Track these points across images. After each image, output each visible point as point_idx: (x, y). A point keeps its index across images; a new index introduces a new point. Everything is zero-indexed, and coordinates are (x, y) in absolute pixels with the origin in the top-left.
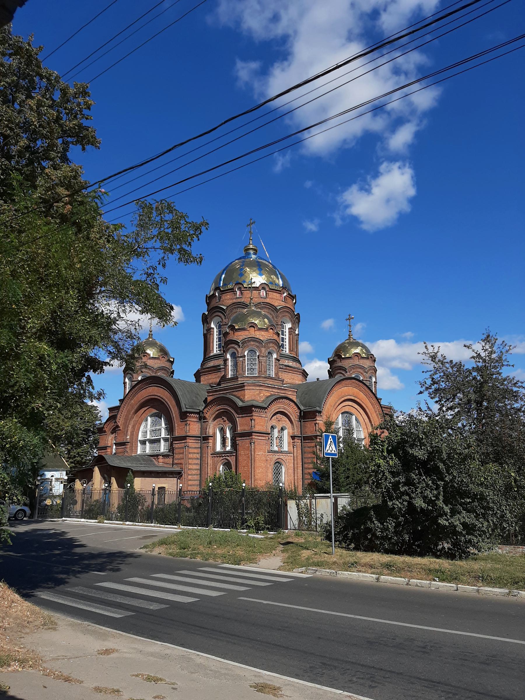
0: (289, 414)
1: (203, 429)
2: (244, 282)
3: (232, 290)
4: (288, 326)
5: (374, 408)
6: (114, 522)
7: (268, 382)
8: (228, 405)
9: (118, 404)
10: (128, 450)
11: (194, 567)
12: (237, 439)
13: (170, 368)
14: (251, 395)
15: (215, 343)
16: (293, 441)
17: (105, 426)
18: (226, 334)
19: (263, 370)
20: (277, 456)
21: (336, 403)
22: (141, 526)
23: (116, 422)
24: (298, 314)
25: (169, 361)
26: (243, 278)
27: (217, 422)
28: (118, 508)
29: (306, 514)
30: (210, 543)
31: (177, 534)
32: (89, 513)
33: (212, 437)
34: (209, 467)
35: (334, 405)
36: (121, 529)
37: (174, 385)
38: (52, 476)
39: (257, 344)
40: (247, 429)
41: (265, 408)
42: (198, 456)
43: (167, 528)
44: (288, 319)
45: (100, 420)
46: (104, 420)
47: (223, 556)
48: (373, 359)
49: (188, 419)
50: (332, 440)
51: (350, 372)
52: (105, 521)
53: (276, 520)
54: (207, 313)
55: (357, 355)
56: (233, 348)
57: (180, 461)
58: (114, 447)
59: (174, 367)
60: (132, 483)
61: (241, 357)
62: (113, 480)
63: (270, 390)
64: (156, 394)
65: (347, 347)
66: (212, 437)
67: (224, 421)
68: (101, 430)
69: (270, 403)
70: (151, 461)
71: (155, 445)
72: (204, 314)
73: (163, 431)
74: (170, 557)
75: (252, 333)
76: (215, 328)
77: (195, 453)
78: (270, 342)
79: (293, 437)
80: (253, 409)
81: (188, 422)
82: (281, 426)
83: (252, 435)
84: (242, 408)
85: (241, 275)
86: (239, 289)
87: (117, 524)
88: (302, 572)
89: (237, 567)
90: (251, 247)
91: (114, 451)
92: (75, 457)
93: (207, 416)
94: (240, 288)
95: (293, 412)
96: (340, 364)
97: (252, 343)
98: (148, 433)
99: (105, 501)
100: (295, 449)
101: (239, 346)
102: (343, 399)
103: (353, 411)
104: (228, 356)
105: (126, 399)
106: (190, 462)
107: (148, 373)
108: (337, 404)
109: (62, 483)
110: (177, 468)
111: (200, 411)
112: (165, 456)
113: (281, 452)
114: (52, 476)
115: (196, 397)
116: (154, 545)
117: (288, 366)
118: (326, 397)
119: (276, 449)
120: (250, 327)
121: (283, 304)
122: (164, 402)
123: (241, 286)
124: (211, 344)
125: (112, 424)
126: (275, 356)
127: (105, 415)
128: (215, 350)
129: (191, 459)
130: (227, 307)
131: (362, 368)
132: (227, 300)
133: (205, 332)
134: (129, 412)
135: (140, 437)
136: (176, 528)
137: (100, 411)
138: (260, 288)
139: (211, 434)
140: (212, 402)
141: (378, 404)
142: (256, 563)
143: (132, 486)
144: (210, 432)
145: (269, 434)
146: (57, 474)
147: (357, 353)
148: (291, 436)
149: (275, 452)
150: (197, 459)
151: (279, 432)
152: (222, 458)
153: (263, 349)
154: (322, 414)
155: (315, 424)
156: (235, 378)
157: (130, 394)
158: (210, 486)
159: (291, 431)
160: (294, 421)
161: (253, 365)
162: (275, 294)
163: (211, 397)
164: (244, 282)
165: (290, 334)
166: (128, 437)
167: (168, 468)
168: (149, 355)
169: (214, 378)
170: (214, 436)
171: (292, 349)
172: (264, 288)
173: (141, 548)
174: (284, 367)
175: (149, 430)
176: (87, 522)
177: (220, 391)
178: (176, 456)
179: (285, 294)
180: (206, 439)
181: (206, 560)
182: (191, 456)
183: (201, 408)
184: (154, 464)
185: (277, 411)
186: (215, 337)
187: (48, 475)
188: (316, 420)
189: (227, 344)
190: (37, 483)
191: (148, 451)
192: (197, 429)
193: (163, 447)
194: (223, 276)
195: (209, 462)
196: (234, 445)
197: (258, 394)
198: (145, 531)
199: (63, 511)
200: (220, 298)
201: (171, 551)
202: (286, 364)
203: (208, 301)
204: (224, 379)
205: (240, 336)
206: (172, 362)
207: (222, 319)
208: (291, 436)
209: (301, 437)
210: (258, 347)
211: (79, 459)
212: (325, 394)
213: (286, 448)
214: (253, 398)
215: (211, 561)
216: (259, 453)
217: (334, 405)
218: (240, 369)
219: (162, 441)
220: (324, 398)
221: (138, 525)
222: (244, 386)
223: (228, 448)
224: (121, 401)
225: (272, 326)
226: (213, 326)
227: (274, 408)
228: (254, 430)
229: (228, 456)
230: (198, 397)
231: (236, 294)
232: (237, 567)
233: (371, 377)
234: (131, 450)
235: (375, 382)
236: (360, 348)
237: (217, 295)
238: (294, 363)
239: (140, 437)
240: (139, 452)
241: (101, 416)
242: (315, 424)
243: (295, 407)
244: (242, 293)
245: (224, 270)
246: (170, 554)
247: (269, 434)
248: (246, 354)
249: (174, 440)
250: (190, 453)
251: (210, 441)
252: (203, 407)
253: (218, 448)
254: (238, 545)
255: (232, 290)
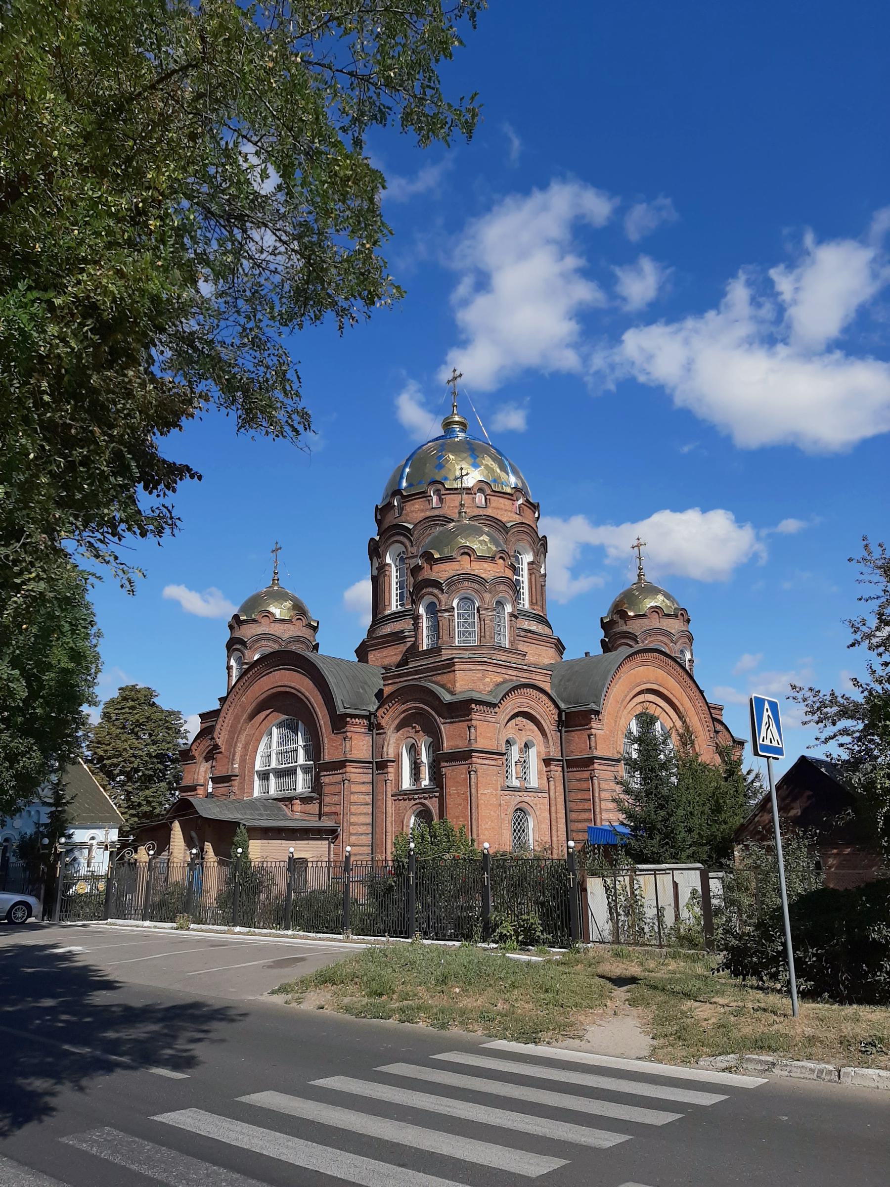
0: (538, 717)
1: (378, 748)
2: (446, 479)
3: (423, 495)
4: (527, 558)
5: (694, 706)
6: (211, 927)
7: (498, 657)
8: (426, 702)
9: (217, 706)
10: (235, 789)
11: (421, 1052)
12: (443, 764)
13: (311, 639)
14: (467, 681)
15: (394, 592)
16: (548, 769)
17: (194, 747)
18: (416, 570)
19: (487, 633)
20: (517, 798)
21: (626, 696)
22: (266, 935)
23: (213, 738)
24: (545, 537)
25: (309, 626)
26: (443, 472)
27: (403, 734)
28: (218, 898)
29: (626, 908)
30: (443, 980)
31: (359, 958)
32: (161, 910)
33: (393, 762)
34: (389, 819)
35: (623, 700)
36: (223, 944)
37: (320, 665)
38: (93, 838)
39: (476, 586)
40: (461, 745)
41: (494, 706)
42: (369, 799)
43: (320, 939)
44: (527, 546)
45: (186, 738)
46: (191, 737)
47: (485, 1017)
48: (686, 618)
49: (348, 728)
50: (770, 713)
51: (643, 642)
52: (192, 926)
53: (563, 920)
54: (377, 538)
55: (656, 610)
56: (431, 594)
57: (333, 809)
58: (210, 783)
59: (319, 638)
60: (246, 848)
61: (446, 611)
62: (208, 847)
63: (503, 671)
64: (287, 683)
65: (637, 597)
66: (393, 762)
67: (417, 732)
68: (186, 756)
69: (504, 696)
70: (280, 809)
71: (287, 779)
72: (372, 539)
73: (301, 753)
74: (348, 1017)
75: (466, 565)
76: (393, 566)
77: (361, 793)
78: (499, 583)
79: (547, 762)
80: (473, 706)
81: (348, 734)
82: (524, 740)
83: (471, 757)
84: (450, 704)
85: (440, 466)
86: (437, 491)
87: (217, 932)
88: (729, 1070)
89: (530, 1049)
90: (457, 418)
91: (210, 790)
92: (140, 805)
93: (383, 722)
94: (438, 490)
95: (547, 714)
96: (624, 628)
97: (466, 584)
98: (274, 757)
99: (191, 883)
100: (552, 783)
101: (442, 590)
102: (638, 689)
103: (658, 712)
104: (422, 611)
105: (232, 695)
106: (353, 810)
107: (271, 647)
108: (628, 698)
109: (106, 849)
110: (327, 823)
111: (371, 714)
112: (305, 800)
113: (527, 790)
114: (93, 838)
115: (363, 689)
116: (304, 984)
117: (530, 631)
118: (607, 685)
119: (516, 783)
120: (462, 554)
121: (518, 519)
122: (303, 697)
123: (440, 486)
124: (387, 594)
125: (206, 743)
126: (509, 608)
127: (193, 726)
128: (394, 606)
129: (355, 803)
130: (416, 525)
131: (667, 634)
132: (416, 512)
133: (375, 573)
134: (237, 718)
135: (258, 766)
136: (340, 941)
137: (186, 722)
138: (476, 490)
139: (391, 756)
140: (392, 696)
141: (701, 700)
142: (580, 1038)
143: (245, 854)
144: (390, 752)
145: (503, 754)
146: (100, 835)
147: (656, 607)
148: (544, 760)
149: (514, 789)
150: (367, 804)
151: (521, 750)
152: (413, 802)
153: (487, 596)
154: (600, 717)
155: (589, 736)
156: (435, 650)
157: (239, 686)
158: (411, 850)
159: (543, 750)
160: (547, 731)
161: (469, 625)
162: (501, 500)
163: (390, 687)
164: (446, 479)
165: (530, 574)
166: (236, 766)
167: (314, 823)
168: (273, 614)
169: (392, 655)
170: (397, 760)
171: (534, 601)
172: (481, 490)
173: (273, 992)
174: (523, 634)
175: (272, 750)
176: (155, 927)
177: (408, 674)
178: (327, 799)
179: (521, 501)
180: (382, 766)
181: (444, 1026)
182: (354, 798)
183: (373, 708)
184: (285, 815)
185: (516, 711)
186: (394, 580)
187: (80, 835)
188: (591, 728)
189: (419, 587)
190: (59, 850)
191: (272, 791)
192: (365, 747)
193: (301, 784)
194: (407, 470)
195: (389, 810)
196: (437, 776)
197: (481, 680)
198: (277, 948)
199: (109, 905)
200: (401, 509)
201: (347, 1000)
202: (525, 627)
203: (379, 517)
204: (413, 652)
205: (442, 572)
206: (315, 629)
207: (406, 547)
208: (544, 760)
209: (562, 761)
210: (477, 591)
211: (146, 808)
212: (605, 679)
213: (534, 781)
214: (471, 686)
215: (455, 1031)
216: (486, 792)
217: (623, 700)
218: (444, 633)
219: (300, 775)
220: (604, 685)
221: (260, 935)
222: (453, 664)
223: (425, 782)
224: (223, 700)
225: (503, 554)
226: (388, 560)
227: (512, 705)
228: (475, 747)
229: (425, 798)
230: (366, 687)
231: (430, 502)
232: (530, 1049)
233: (682, 652)
234: (242, 789)
235: (690, 661)
236: (660, 597)
237: (396, 504)
238: (540, 626)
239: (258, 766)
240: (256, 793)
241: (187, 732)
242: (589, 736)
243: (550, 703)
244: (441, 500)
245: (408, 460)
246: (348, 1009)
247: (503, 754)
248: (455, 604)
249: (322, 768)
250: (352, 793)
251: (391, 770)
252: (375, 707)
253: (407, 783)
254: (513, 986)
255: (423, 495)
